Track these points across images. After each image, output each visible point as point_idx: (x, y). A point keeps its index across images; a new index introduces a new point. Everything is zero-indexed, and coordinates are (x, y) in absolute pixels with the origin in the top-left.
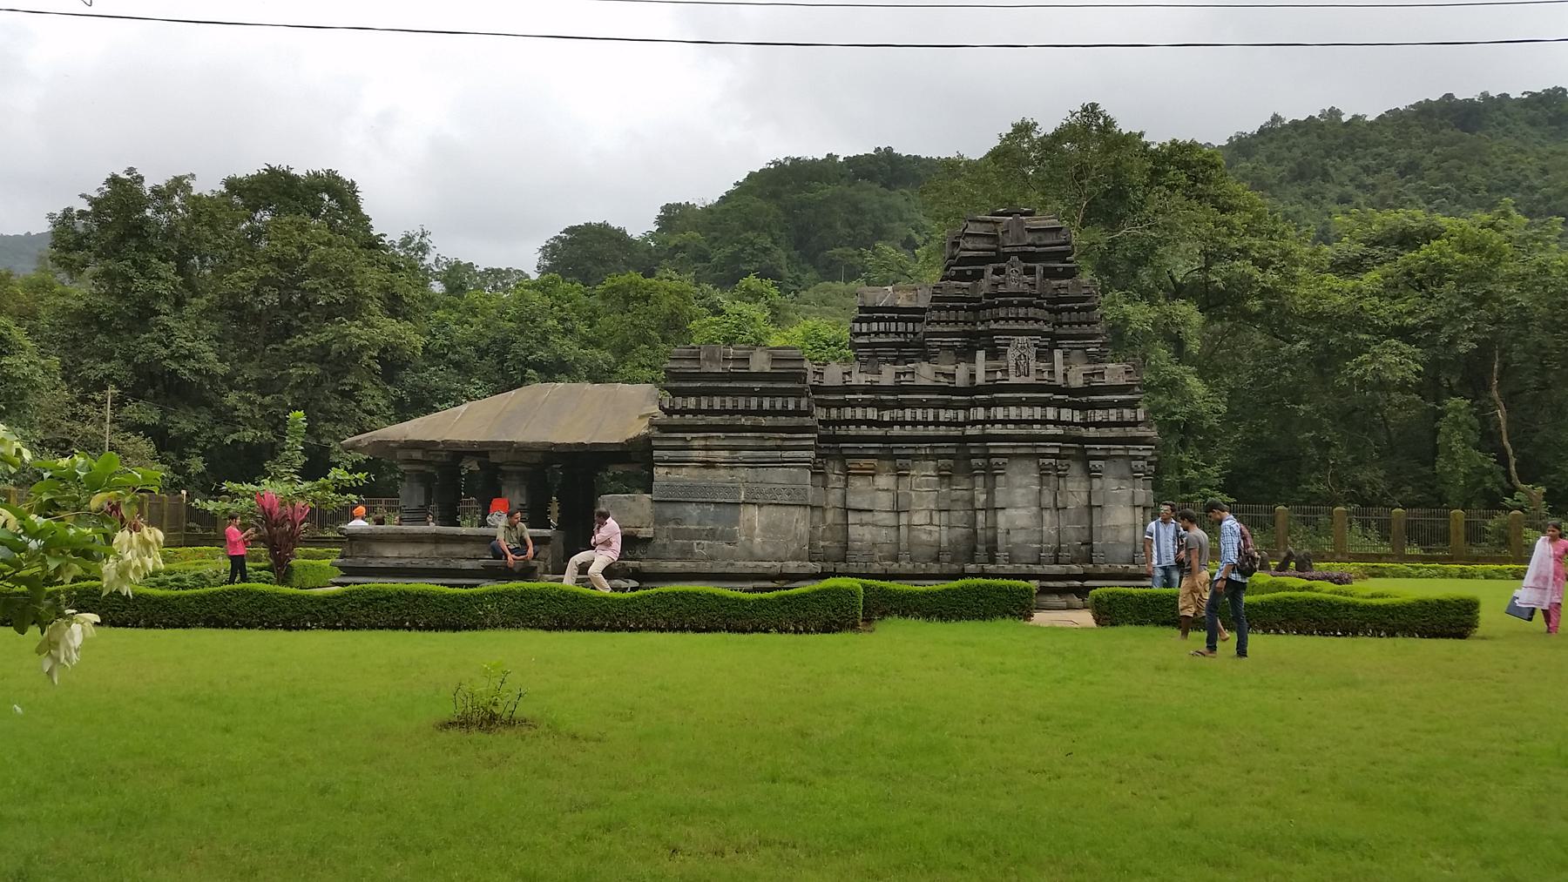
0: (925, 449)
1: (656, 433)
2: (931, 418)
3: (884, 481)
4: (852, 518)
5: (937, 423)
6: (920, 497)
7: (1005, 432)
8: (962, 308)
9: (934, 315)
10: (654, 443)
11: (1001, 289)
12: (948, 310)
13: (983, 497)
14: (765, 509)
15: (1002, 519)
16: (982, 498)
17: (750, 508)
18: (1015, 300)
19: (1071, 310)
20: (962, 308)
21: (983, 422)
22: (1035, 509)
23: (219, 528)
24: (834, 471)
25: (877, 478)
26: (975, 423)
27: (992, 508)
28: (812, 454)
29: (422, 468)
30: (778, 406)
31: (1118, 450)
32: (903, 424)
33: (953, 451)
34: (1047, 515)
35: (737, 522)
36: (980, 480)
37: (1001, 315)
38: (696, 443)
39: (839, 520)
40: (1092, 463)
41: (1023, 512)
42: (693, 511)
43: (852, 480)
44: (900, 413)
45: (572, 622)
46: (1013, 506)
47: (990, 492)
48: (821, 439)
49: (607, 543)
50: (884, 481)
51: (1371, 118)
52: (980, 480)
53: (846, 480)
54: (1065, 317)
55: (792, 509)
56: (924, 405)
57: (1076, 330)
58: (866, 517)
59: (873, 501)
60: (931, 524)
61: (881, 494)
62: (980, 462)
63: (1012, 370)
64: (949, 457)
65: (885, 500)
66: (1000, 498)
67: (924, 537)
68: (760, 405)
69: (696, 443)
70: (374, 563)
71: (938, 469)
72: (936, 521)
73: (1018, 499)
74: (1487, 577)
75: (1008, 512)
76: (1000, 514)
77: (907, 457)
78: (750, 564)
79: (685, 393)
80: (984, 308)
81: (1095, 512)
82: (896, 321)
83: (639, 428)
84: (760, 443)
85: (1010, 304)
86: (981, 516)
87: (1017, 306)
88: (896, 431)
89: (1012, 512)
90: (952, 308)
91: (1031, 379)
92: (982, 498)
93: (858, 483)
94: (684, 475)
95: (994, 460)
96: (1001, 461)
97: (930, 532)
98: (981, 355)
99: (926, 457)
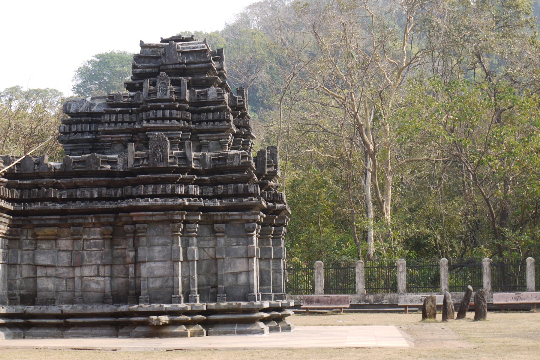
0: (91, 219)
4: (40, 272)
6: (90, 256)
7: (147, 204)
8: (127, 112)
9: (107, 118)
11: (153, 98)
15: (144, 270)
18: (163, 105)
19: (208, 111)
20: (127, 112)
23: (8, 293)
25: (59, 242)
29: (119, 247)
31: (235, 215)
37: (152, 116)
40: (216, 226)
41: (160, 264)
46: (151, 260)
50: (64, 244)
53: (36, 244)
54: (204, 116)
57: (210, 126)
58: (50, 271)
60: (98, 275)
61: (62, 254)
65: (65, 258)
66: (142, 253)
67: (94, 286)
71: (102, 234)
72: (101, 274)
75: (148, 265)
80: (145, 110)
82: (90, 123)
89: (153, 264)
98: (132, 147)
99: (94, 225)
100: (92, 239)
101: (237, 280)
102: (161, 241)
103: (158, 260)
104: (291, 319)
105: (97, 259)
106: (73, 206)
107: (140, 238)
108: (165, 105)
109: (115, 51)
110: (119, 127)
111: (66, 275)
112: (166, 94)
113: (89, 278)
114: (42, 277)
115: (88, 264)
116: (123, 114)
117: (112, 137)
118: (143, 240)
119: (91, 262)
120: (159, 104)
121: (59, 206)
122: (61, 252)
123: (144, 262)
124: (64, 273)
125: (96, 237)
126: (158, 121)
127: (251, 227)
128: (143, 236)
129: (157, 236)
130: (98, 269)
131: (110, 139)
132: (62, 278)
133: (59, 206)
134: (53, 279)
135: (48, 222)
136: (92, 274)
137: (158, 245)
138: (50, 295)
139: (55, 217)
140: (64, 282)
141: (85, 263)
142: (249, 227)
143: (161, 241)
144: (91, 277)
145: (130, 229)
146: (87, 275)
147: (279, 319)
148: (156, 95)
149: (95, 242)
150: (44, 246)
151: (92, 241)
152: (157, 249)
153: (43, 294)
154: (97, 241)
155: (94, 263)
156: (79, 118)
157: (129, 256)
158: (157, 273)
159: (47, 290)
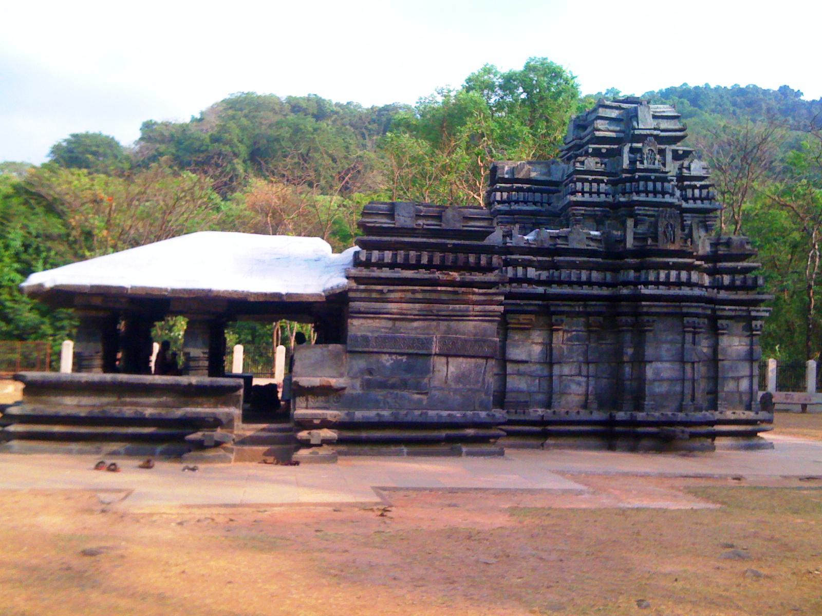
1: (354, 285)
2: (425, 260)
4: (510, 368)
5: (590, 283)
10: (351, 295)
12: (591, 182)
13: (630, 351)
21: (635, 283)
26: (626, 284)
27: (640, 361)
28: (501, 308)
29: (604, 342)
32: (560, 283)
33: (604, 309)
36: (628, 337)
38: (392, 296)
41: (667, 365)
44: (556, 273)
46: (659, 359)
47: (639, 346)
48: (508, 296)
49: (712, 414)
51: (807, 97)
52: (628, 337)
56: (579, 267)
58: (522, 367)
60: (580, 375)
62: (629, 319)
64: (599, 314)
66: (649, 351)
69: (392, 296)
72: (584, 373)
73: (664, 353)
75: (654, 365)
77: (562, 313)
78: (445, 413)
79: (381, 247)
81: (720, 364)
83: (338, 281)
84: (428, 296)
86: (627, 369)
88: (555, 290)
89: (659, 365)
90: (594, 181)
99: (578, 314)
100: (574, 331)
101: (738, 386)
102: (670, 337)
103: (665, 359)
104: (507, 451)
105: (578, 355)
106: (555, 290)
107: (647, 333)
108: (655, 177)
109: (204, 109)
110: (595, 198)
111: (539, 372)
112: (654, 164)
113: (569, 378)
114: (513, 374)
115: (568, 360)
116: (631, 183)
117: (585, 210)
118: (649, 335)
119: (572, 358)
120: (650, 174)
121: (540, 290)
122: (534, 345)
123: (651, 362)
124: (537, 370)
125: (579, 329)
126: (594, 195)
127: (758, 325)
128: (650, 331)
129: (665, 331)
130: (580, 367)
131: (583, 212)
132: (535, 376)
133: (540, 290)
134: (526, 377)
135: (526, 308)
136: (573, 373)
137: (666, 342)
138: (522, 398)
139: (537, 302)
140: (537, 381)
141: (564, 359)
142: (756, 326)
143: (670, 337)
144: (571, 376)
145: (629, 321)
146: (566, 373)
147: (752, 434)
148: (643, 164)
149: (367, 346)
150: (517, 337)
151: (574, 333)
152: (665, 346)
153: (514, 395)
154: (580, 333)
155: (575, 359)
156: (520, 185)
157: (627, 354)
158: (665, 375)
159: (520, 392)
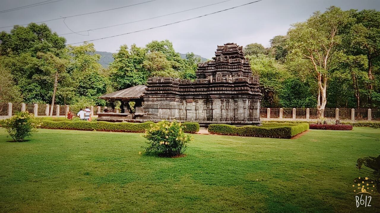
3: (194, 104)
8: (212, 66)
10: (144, 97)
14: (163, 109)
16: (210, 107)
17: (160, 109)
22: (220, 109)
24: (184, 102)
30: (156, 89)
34: (223, 111)
35: (158, 112)
39: (186, 112)
41: (218, 110)
42: (151, 110)
43: (188, 103)
45: (73, 129)
55: (167, 109)
59: (191, 108)
60: (203, 113)
63: (216, 80)
65: (194, 108)
67: (201, 115)
68: (215, 89)
70: (101, 119)
74: (365, 126)
76: (197, 111)
85: (220, 65)
87: (222, 65)
89: (216, 110)
90: (237, 65)
91: (220, 82)
92: (210, 107)
93: (189, 104)
94: (150, 103)
95: (212, 99)
96: (213, 99)
97: (203, 115)
152: (218, 106)
